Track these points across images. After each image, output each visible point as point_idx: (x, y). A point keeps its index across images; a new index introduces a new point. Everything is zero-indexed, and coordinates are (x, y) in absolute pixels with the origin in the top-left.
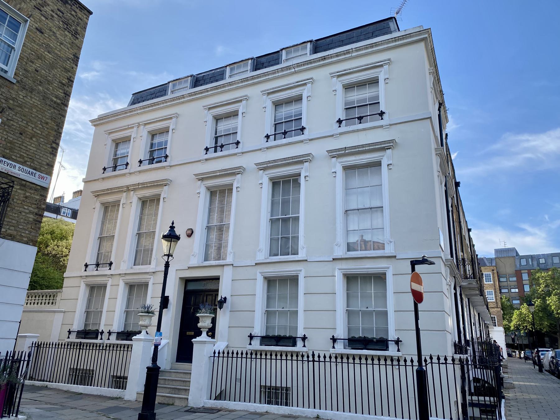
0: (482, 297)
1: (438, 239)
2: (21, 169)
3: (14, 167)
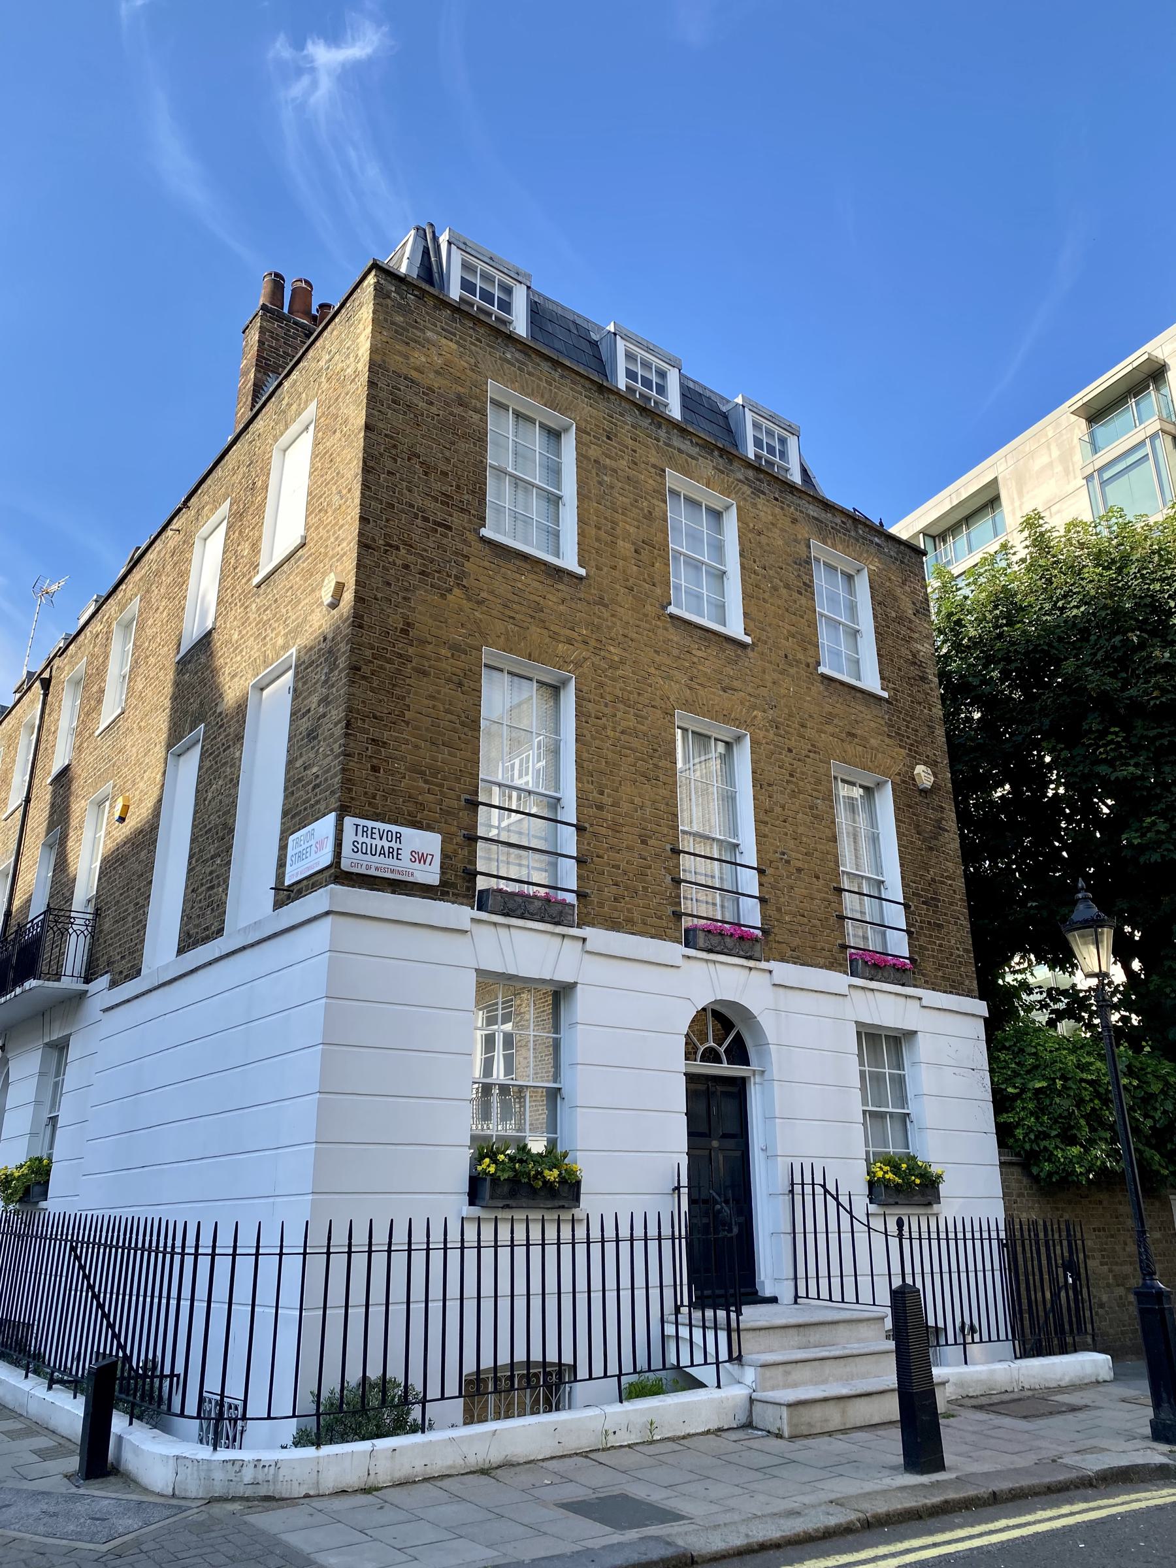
0: (736, 464)
1: (884, 934)
2: (359, 846)
3: (363, 831)
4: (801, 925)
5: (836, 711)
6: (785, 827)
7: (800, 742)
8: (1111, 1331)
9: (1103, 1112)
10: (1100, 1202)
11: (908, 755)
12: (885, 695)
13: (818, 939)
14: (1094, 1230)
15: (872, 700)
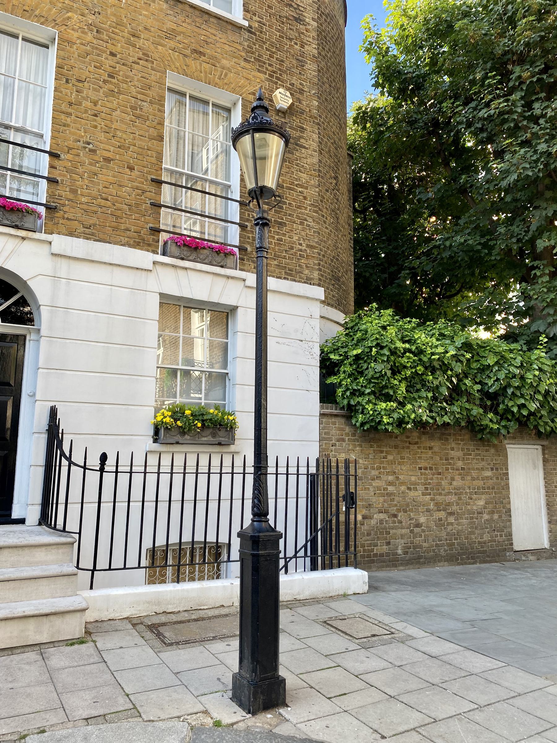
4: (101, 207)
5: (180, 29)
6: (95, 121)
7: (128, 49)
8: (425, 545)
9: (428, 378)
10: (431, 448)
11: (267, 79)
12: (246, 24)
13: (123, 221)
14: (420, 469)
15: (230, 27)
